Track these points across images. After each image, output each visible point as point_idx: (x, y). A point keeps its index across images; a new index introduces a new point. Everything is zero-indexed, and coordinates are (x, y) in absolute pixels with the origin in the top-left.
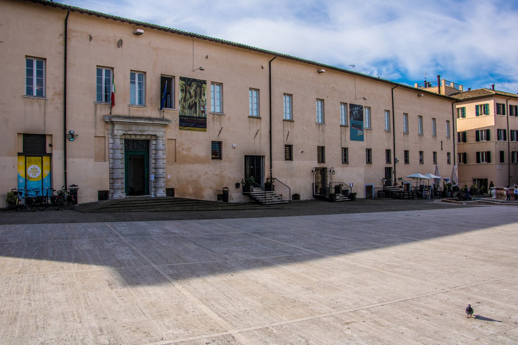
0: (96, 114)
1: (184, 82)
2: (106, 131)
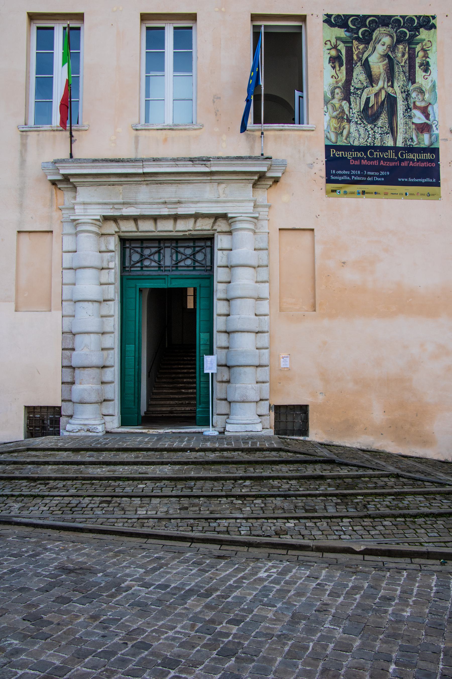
0: (23, 162)
1: (341, 33)
2: (56, 215)
